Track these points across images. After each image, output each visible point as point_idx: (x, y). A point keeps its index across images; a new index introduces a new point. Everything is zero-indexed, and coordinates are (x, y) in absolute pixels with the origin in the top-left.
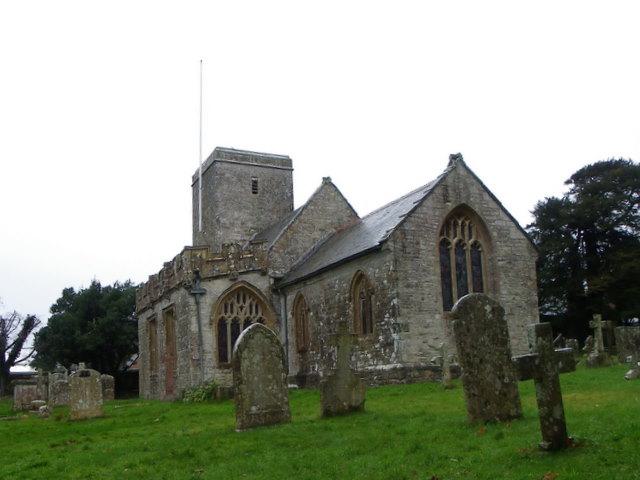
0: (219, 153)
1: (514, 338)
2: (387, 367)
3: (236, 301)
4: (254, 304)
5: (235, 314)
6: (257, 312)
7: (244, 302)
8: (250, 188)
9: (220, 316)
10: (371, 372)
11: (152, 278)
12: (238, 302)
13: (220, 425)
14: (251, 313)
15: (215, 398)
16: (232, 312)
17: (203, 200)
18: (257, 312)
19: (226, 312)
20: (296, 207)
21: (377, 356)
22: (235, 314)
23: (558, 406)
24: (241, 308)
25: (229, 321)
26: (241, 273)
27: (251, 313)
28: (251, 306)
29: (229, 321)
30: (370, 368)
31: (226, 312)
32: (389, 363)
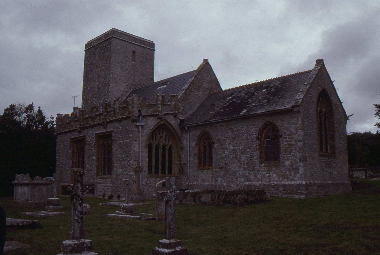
1: (216, 181)
2: (293, 183)
4: (168, 135)
10: (278, 185)
22: (157, 142)
24: (161, 137)
25: (167, 147)
26: (165, 114)
29: (154, 145)
30: (276, 183)
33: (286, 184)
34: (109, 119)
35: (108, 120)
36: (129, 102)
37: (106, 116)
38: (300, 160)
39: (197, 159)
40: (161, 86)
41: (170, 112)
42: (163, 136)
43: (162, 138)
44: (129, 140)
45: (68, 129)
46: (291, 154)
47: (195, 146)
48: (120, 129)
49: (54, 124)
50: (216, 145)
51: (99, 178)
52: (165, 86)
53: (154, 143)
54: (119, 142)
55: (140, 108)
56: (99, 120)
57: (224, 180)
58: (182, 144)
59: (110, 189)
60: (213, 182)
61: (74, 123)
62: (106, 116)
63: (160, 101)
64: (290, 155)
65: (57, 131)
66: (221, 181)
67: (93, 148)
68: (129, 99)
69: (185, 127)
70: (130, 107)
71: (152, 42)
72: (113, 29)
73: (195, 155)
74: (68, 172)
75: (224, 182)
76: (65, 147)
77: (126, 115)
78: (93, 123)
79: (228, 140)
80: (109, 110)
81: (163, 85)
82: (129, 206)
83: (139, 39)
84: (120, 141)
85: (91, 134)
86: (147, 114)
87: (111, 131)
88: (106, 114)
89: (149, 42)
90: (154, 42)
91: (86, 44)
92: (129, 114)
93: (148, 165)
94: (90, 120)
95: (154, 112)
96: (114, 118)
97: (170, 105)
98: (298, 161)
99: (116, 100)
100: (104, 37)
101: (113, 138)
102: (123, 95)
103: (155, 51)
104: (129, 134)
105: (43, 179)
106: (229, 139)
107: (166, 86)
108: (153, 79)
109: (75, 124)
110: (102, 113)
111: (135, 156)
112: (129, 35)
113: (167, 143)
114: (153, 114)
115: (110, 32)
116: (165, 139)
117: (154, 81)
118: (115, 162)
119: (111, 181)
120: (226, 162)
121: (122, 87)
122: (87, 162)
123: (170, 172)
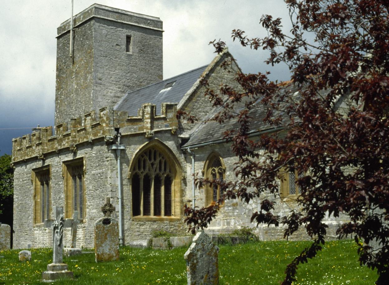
0: (162, 22)
1: (228, 223)
3: (148, 159)
5: (147, 171)
6: (165, 170)
7: (155, 159)
9: (135, 172)
11: (56, 87)
12: (150, 159)
13: (235, 161)
14: (160, 169)
15: (316, 31)
16: (144, 168)
17: (131, 22)
18: (165, 170)
19: (139, 169)
20: (166, 76)
23: (326, 229)
24: (152, 164)
25: (142, 177)
27: (160, 169)
28: (160, 162)
29: (142, 177)
31: (139, 169)
34: (79, 141)
35: (77, 143)
36: (102, 117)
37: (76, 138)
39: (204, 193)
40: (165, 88)
41: (164, 129)
42: (155, 163)
43: (155, 166)
44: (104, 170)
45: (28, 156)
48: (94, 155)
49: (338, 95)
51: (37, 226)
52: (169, 89)
53: (142, 173)
54: (92, 172)
55: (118, 126)
57: (239, 221)
58: (186, 172)
59: (82, 238)
60: (225, 226)
61: (36, 148)
62: (75, 137)
63: (147, 114)
65: (14, 160)
66: (235, 223)
67: (60, 181)
68: (103, 114)
69: (187, 149)
70: (104, 125)
71: (159, 18)
72: (95, 5)
74: (30, 217)
75: (239, 225)
76: (25, 182)
77: (100, 135)
78: (59, 148)
80: (79, 129)
81: (167, 87)
82: (74, 250)
83: (136, 17)
84: (92, 170)
85: (58, 163)
86: (129, 133)
87: (82, 158)
88: (75, 134)
89: (154, 19)
90: (161, 19)
91: (58, 27)
92: (103, 134)
93: (131, 203)
94: (56, 142)
95: (139, 130)
96: (85, 140)
97: (165, 119)
99: (87, 115)
100: (82, 17)
101: (84, 168)
102: (114, 102)
103: (163, 33)
104: (104, 162)
107: (171, 88)
108: (161, 76)
109: (37, 149)
110: (70, 134)
111: (111, 191)
112: (120, 11)
113: (140, 172)
114: (139, 132)
115: (90, 10)
116: (158, 166)
117: (162, 79)
118: (88, 200)
119: (83, 226)
121: (110, 91)
122: (53, 202)
123: (168, 212)
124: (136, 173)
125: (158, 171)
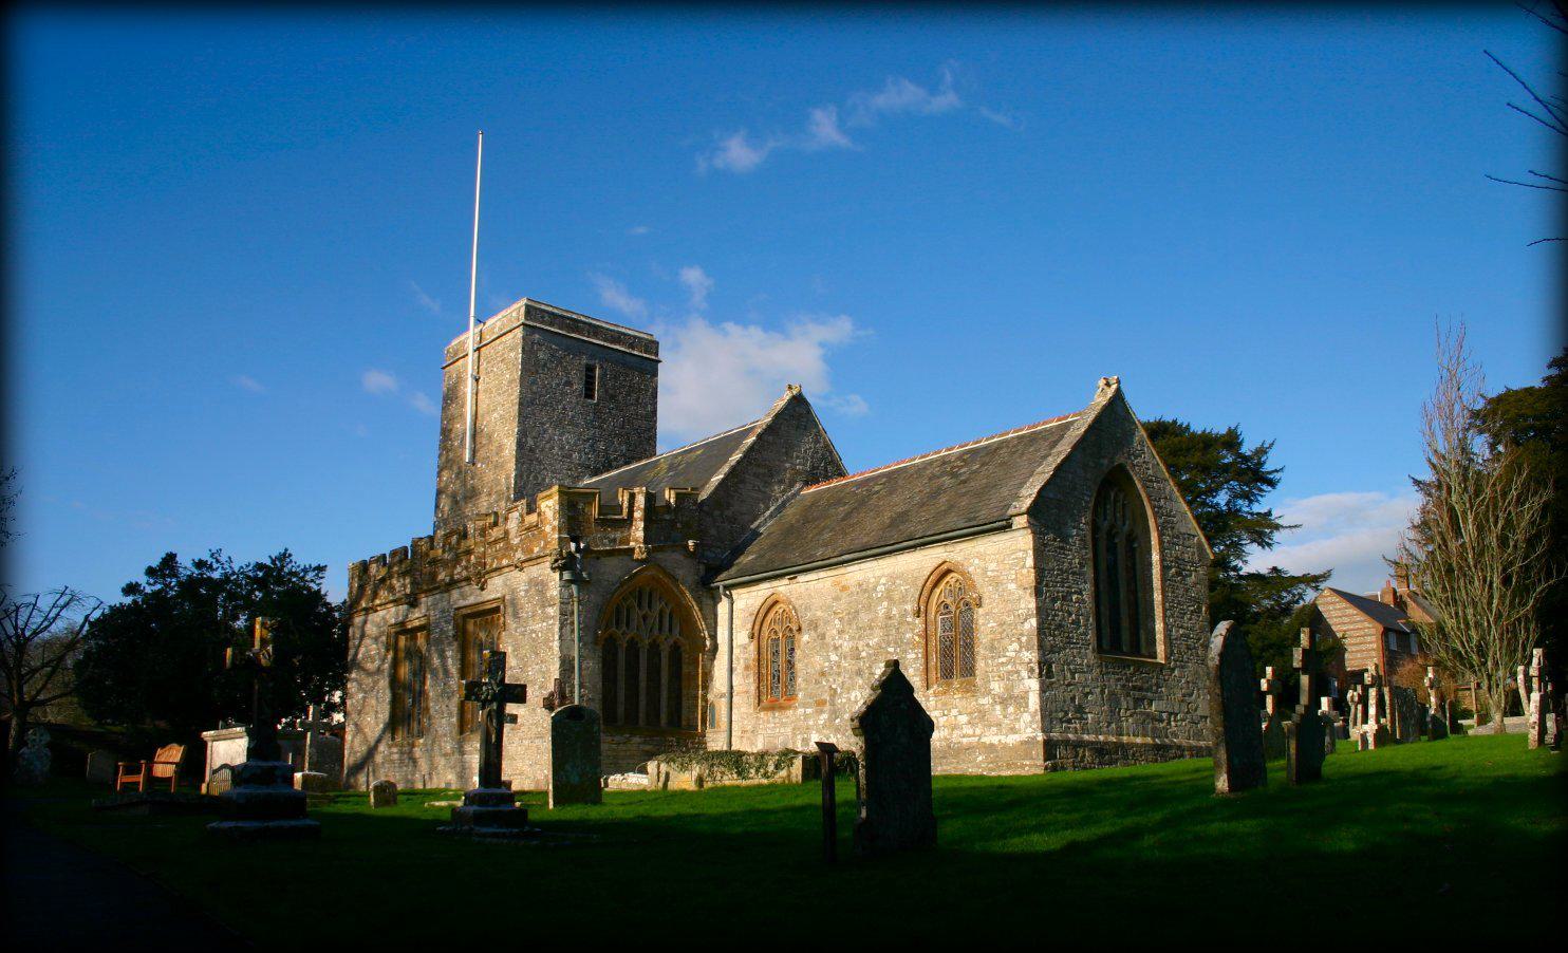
8: (578, 386)
12: (640, 605)
21: (981, 716)
24: (645, 618)
30: (965, 740)
32: (1013, 730)
33: (993, 742)
38: (1031, 670)
46: (1007, 654)
47: (747, 640)
50: (805, 638)
56: (466, 568)
64: (1003, 660)
73: (747, 668)
79: (837, 622)
98: (1024, 674)
105: (637, 723)
106: (841, 619)
120: (834, 686)
124: (611, 636)
125: (656, 632)
